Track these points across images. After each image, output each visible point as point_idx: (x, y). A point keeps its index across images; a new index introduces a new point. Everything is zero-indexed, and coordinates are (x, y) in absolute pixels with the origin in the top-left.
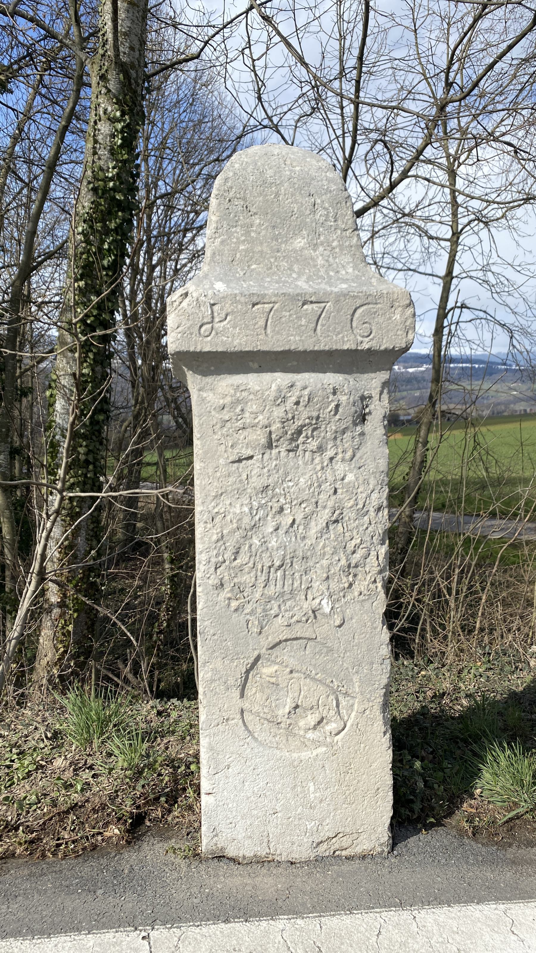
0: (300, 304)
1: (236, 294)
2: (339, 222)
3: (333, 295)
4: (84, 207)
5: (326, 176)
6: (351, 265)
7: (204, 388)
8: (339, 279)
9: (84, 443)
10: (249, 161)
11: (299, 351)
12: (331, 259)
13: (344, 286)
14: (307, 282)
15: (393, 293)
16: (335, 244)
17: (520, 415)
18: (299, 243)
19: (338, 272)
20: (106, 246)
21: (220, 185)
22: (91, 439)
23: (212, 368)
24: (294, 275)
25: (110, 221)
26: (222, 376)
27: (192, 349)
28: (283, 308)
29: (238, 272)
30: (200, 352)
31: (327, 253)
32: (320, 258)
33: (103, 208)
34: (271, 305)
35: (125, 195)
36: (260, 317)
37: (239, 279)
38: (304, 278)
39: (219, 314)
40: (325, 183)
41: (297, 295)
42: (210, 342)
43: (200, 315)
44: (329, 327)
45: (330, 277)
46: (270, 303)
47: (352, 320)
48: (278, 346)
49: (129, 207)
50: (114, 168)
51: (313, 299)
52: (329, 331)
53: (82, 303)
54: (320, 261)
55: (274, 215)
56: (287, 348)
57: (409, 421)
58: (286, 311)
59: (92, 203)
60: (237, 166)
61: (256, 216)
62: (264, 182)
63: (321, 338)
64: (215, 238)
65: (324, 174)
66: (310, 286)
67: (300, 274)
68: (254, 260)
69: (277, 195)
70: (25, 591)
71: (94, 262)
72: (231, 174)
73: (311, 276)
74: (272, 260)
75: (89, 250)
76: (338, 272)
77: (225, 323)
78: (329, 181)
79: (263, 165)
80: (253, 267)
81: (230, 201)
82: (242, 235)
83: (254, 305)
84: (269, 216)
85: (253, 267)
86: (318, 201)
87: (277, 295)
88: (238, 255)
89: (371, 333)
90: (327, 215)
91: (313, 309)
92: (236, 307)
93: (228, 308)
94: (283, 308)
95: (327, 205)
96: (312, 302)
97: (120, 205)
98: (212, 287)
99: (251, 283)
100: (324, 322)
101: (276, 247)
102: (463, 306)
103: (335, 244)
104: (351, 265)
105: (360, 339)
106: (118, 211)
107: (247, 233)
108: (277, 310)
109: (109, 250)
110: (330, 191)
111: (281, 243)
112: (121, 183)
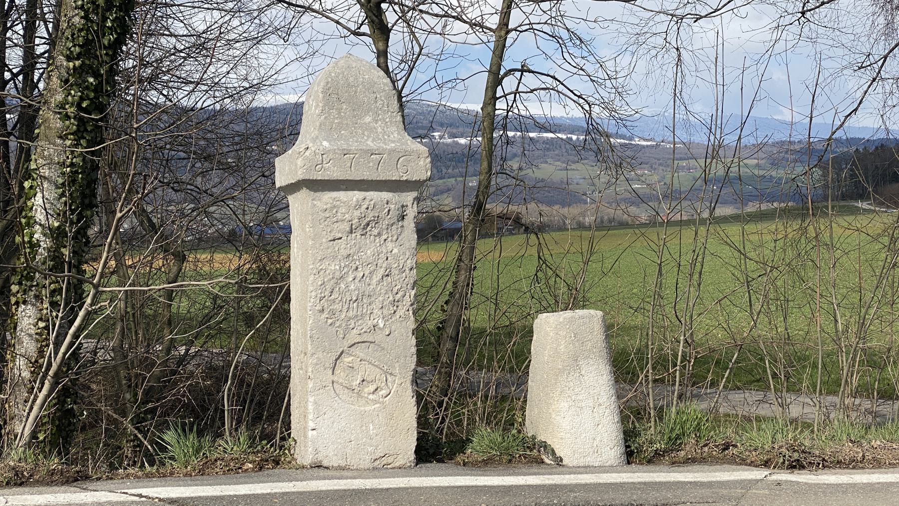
18: (368, 119)
28: (360, 156)
45: (385, 139)
62: (349, 85)
67: (368, 137)
69: (356, 92)
93: (331, 156)
102: (524, 70)
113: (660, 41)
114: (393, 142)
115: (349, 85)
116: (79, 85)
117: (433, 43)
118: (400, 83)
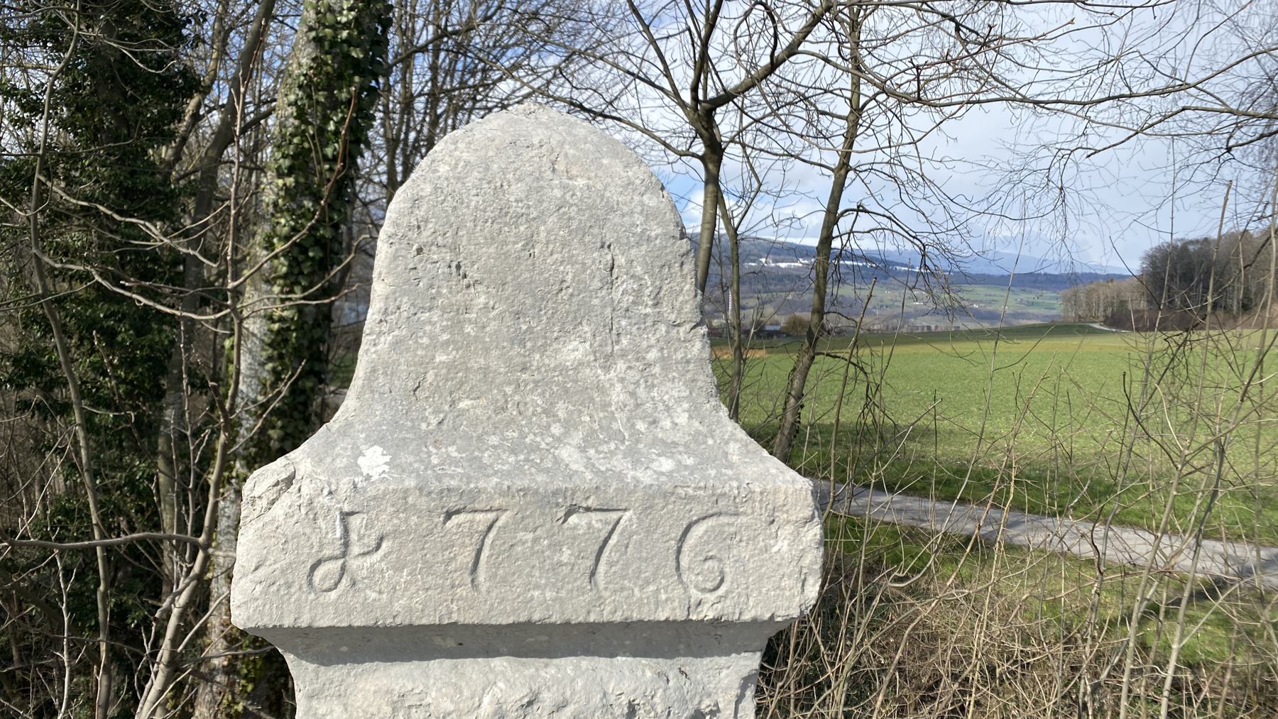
0: (561, 514)
1: (406, 491)
2: (665, 308)
4: (300, 65)
5: (643, 205)
6: (686, 406)
7: (322, 690)
8: (655, 442)
9: (279, 423)
10: (472, 159)
11: (553, 625)
12: (641, 391)
13: (666, 465)
14: (583, 450)
17: (922, 334)
18: (574, 351)
19: (654, 422)
20: (331, 127)
21: (401, 214)
22: (292, 417)
23: (345, 649)
24: (556, 430)
25: (340, 90)
26: (367, 665)
27: (287, 622)
28: (520, 522)
29: (425, 419)
30: (310, 627)
31: (633, 375)
32: (618, 387)
33: (329, 69)
34: (491, 516)
35: (366, 53)
36: (463, 545)
37: (423, 439)
38: (577, 437)
39: (360, 538)
40: (639, 219)
41: (555, 493)
43: (315, 540)
44: (626, 566)
45: (636, 436)
46: (490, 510)
47: (679, 551)
49: (373, 68)
50: (350, 9)
52: (624, 577)
53: (288, 210)
55: (519, 287)
56: (523, 618)
57: (777, 333)
58: (525, 529)
59: (314, 60)
60: (443, 169)
61: (480, 288)
62: (503, 212)
64: (380, 333)
65: (637, 198)
66: (590, 465)
67: (569, 425)
68: (467, 387)
69: (530, 242)
70: (147, 686)
71: (310, 150)
72: (428, 189)
73: (593, 431)
74: (509, 390)
75: (304, 131)
76: (654, 422)
78: (648, 215)
79: (504, 171)
80: (462, 405)
81: (420, 251)
82: (443, 330)
83: (449, 515)
84: (509, 289)
85: (462, 405)
86: (621, 260)
88: (430, 377)
89: (722, 581)
90: (638, 293)
91: (589, 526)
92: (406, 520)
93: (385, 522)
94: (520, 522)
95: (639, 270)
96: (588, 509)
97: (357, 67)
98: (353, 468)
99: (452, 451)
100: (615, 556)
101: (518, 360)
102: (860, 209)
103: (652, 355)
104: (686, 406)
105: (695, 595)
106: (354, 74)
107: (457, 325)
109: (337, 133)
110: (649, 239)
111: (533, 350)
112: (361, 33)
113: (1039, 178)
114: (668, 448)
115: (503, 212)
116: (291, 212)
117: (772, 180)
118: (736, 221)
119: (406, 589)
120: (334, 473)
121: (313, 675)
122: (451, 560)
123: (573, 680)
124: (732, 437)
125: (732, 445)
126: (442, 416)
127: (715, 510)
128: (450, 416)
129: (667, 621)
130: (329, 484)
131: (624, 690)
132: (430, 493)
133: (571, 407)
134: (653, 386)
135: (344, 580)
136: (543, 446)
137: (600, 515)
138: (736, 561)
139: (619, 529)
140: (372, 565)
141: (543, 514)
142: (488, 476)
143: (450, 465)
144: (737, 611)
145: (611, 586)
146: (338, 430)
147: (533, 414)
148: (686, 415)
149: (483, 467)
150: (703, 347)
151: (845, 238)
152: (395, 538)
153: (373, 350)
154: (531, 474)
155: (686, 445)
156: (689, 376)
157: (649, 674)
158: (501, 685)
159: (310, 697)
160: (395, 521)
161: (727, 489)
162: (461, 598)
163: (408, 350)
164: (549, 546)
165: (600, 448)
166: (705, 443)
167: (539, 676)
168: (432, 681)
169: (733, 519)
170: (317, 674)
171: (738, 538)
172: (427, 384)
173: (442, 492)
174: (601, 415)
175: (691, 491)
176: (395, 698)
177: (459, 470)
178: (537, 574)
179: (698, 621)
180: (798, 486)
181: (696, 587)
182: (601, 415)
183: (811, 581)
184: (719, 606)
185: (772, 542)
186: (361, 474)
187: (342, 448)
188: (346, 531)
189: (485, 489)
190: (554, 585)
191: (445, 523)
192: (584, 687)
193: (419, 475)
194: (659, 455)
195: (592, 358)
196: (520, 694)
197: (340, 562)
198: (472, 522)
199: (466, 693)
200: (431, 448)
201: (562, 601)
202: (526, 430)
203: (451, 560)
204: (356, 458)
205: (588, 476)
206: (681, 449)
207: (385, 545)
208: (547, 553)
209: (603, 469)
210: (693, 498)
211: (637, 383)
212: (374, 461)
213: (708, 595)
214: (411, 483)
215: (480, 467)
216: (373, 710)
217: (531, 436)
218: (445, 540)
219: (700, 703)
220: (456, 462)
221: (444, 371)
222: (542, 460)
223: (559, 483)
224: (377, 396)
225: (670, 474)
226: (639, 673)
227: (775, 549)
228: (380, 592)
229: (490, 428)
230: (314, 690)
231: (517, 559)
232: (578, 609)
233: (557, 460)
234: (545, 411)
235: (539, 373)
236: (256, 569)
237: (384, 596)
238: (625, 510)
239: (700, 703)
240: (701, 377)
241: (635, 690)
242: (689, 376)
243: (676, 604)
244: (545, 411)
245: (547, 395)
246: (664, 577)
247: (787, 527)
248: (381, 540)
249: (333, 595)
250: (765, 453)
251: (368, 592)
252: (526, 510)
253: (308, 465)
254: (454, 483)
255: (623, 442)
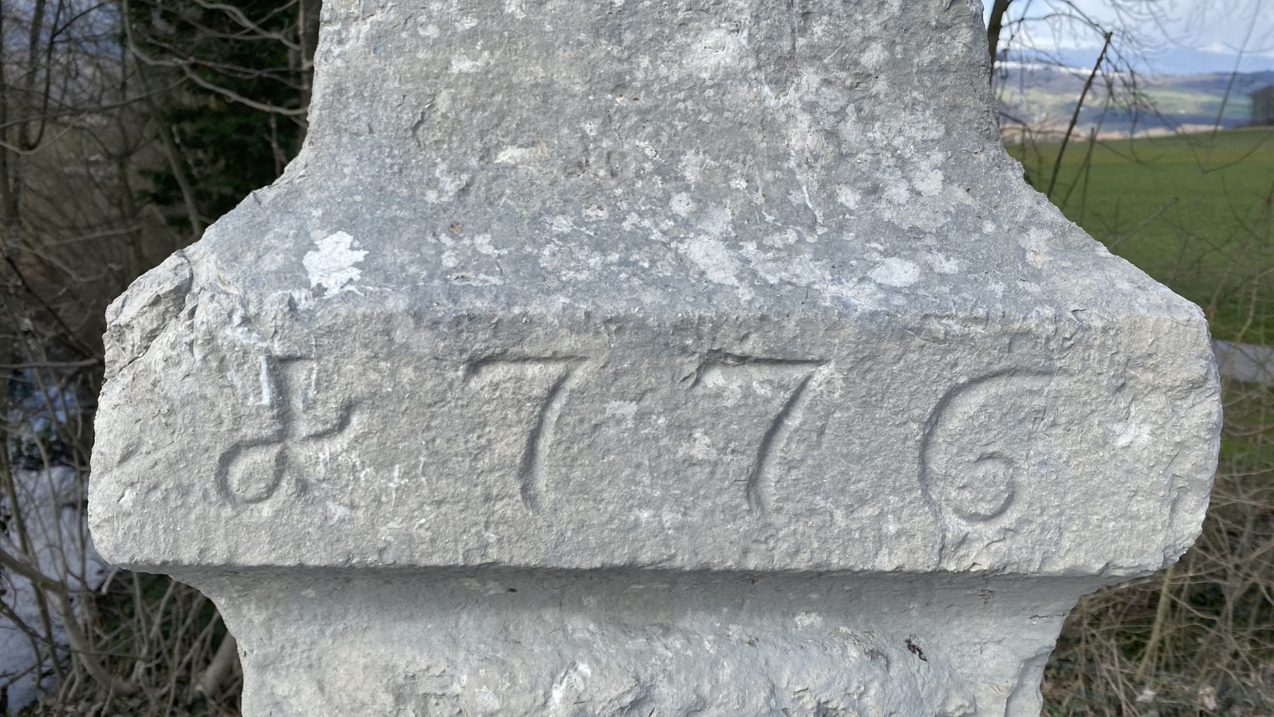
1: (389, 318)
3: (850, 331)
6: (938, 157)
7: (280, 657)
8: (878, 228)
14: (733, 244)
15: (1135, 328)
16: (873, 56)
24: (681, 205)
28: (611, 381)
29: (433, 183)
31: (833, 98)
32: (804, 120)
34: (555, 369)
36: (504, 423)
37: (430, 219)
38: (721, 220)
39: (309, 406)
41: (681, 327)
42: (271, 525)
45: (839, 218)
46: (554, 358)
47: (925, 444)
48: (582, 548)
51: (753, 346)
52: (815, 490)
54: (802, 137)
58: (622, 396)
63: (780, 520)
66: (747, 273)
67: (705, 197)
68: (511, 123)
74: (591, 128)
77: (340, 442)
83: (475, 365)
87: (583, 325)
88: (443, 102)
89: (1010, 501)
91: (747, 392)
92: (393, 373)
93: (353, 375)
94: (611, 381)
96: (743, 360)
98: (294, 273)
99: (483, 243)
100: (797, 451)
104: (938, 157)
105: (955, 525)
108: (580, 392)
111: (634, 50)
114: (904, 240)
119: (400, 502)
120: (254, 281)
121: (262, 631)
122: (482, 449)
123: (714, 664)
124: (1033, 219)
125: (1033, 233)
126: (465, 177)
127: (1004, 364)
128: (482, 177)
129: (898, 570)
130: (245, 304)
131: (809, 683)
132: (435, 324)
133: (710, 162)
134: (873, 118)
135: (284, 483)
136: (656, 235)
137: (767, 372)
138: (1044, 463)
139: (806, 399)
140: (334, 457)
141: (656, 368)
142: (548, 292)
143: (477, 270)
144: (1038, 556)
145: (789, 506)
146: (274, 203)
147: (638, 176)
148: (939, 175)
149: (538, 275)
150: (975, 41)
151: (1015, 26)
152: (374, 407)
153: (336, 51)
154: (632, 290)
155: (940, 235)
156: (945, 98)
157: (853, 653)
158: (584, 668)
159: (262, 667)
160: (373, 376)
161: (1032, 323)
162: (503, 520)
163: (399, 50)
164: (670, 427)
165: (768, 241)
166: (978, 230)
167: (653, 653)
168: (462, 654)
169: (1036, 383)
170: (269, 631)
171: (1048, 419)
172: (437, 117)
173: (458, 321)
174: (769, 176)
175: (956, 328)
176: (401, 680)
177: (495, 280)
178: (647, 481)
179: (957, 574)
180: (1182, 318)
181: (957, 511)
182: (769, 176)
183: (1191, 500)
184: (1002, 547)
185: (1118, 428)
186: (307, 284)
187: (278, 236)
188: (282, 389)
189: (543, 317)
190: (677, 500)
191: (466, 380)
192: (735, 677)
193: (415, 288)
194: (886, 254)
195: (752, 63)
196: (617, 690)
197: (275, 450)
198: (519, 379)
199: (522, 680)
200: (444, 238)
201: (694, 531)
202: (624, 206)
203: (482, 449)
204: (301, 254)
205: (745, 294)
206: (930, 241)
207: (357, 421)
208: (665, 441)
209: (773, 280)
210: (964, 339)
211: (841, 114)
212: (334, 260)
213: (980, 526)
214: (398, 303)
215: (534, 275)
216: (363, 696)
217: (633, 218)
218: (468, 413)
219: (944, 704)
220: (487, 265)
221: (468, 91)
222: (653, 263)
223: (686, 309)
224: (345, 139)
225: (911, 292)
226: (836, 652)
227: (1123, 441)
228: (353, 507)
229: (554, 203)
230: (266, 656)
231: (608, 451)
232: (723, 548)
233: (682, 262)
234: (659, 170)
235: (649, 94)
236: (124, 459)
237: (360, 513)
238: (820, 362)
239: (944, 704)
240: (970, 101)
241: (828, 686)
242: (945, 98)
243: (918, 541)
244: (659, 170)
245: (664, 139)
246: (894, 491)
247: (1153, 398)
248: (348, 409)
249: (266, 509)
250: (1102, 251)
251: (330, 504)
252: (623, 358)
253: (212, 266)
254: (481, 305)
255: (812, 228)
